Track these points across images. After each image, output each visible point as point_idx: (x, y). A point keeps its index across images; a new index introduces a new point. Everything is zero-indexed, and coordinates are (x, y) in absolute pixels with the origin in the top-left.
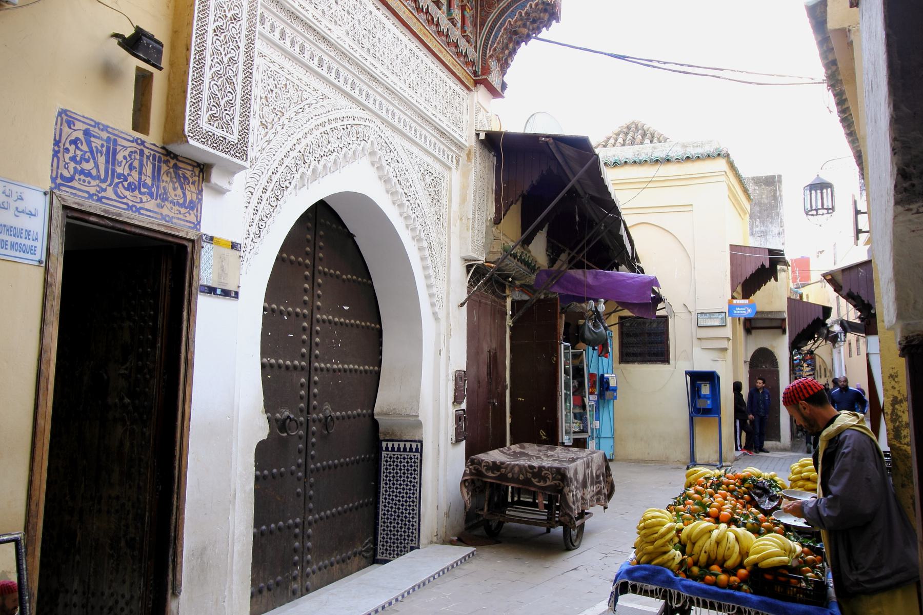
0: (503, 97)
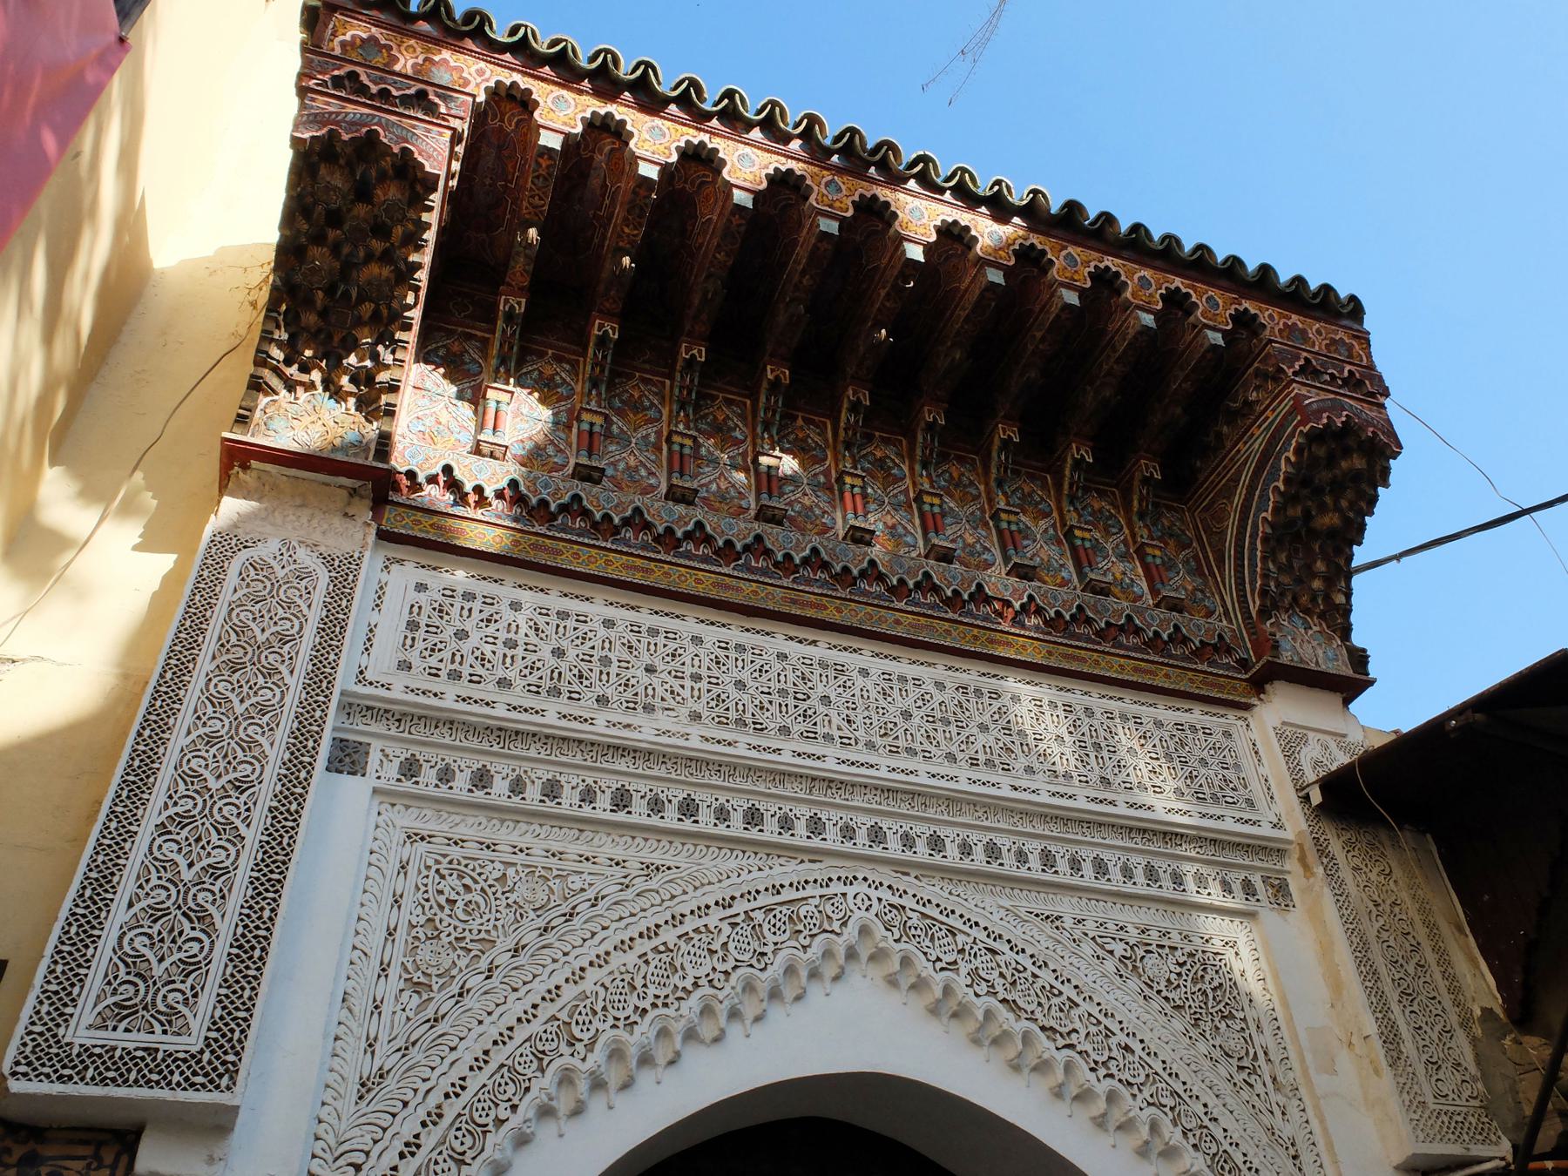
0: (1371, 683)
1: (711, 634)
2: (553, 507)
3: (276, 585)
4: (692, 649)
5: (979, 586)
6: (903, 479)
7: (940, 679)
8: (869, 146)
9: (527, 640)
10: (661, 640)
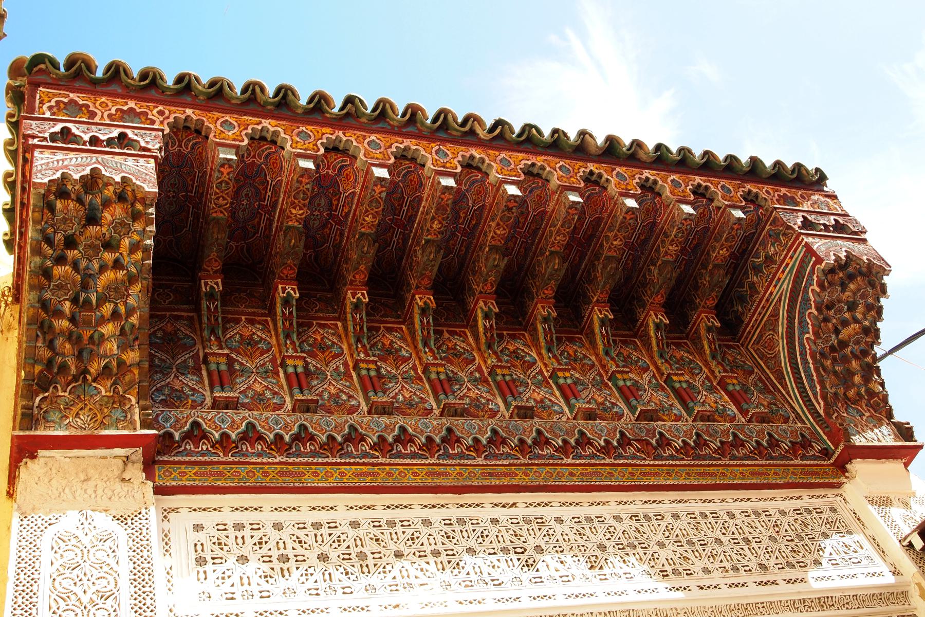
1: (435, 515)
2: (287, 438)
3: (85, 551)
4: (425, 530)
5: (622, 434)
6: (535, 363)
7: (616, 513)
8: (460, 120)
9: (295, 552)
10: (398, 528)
